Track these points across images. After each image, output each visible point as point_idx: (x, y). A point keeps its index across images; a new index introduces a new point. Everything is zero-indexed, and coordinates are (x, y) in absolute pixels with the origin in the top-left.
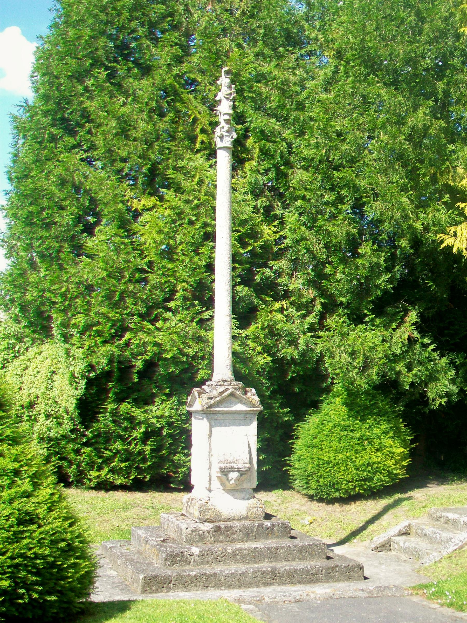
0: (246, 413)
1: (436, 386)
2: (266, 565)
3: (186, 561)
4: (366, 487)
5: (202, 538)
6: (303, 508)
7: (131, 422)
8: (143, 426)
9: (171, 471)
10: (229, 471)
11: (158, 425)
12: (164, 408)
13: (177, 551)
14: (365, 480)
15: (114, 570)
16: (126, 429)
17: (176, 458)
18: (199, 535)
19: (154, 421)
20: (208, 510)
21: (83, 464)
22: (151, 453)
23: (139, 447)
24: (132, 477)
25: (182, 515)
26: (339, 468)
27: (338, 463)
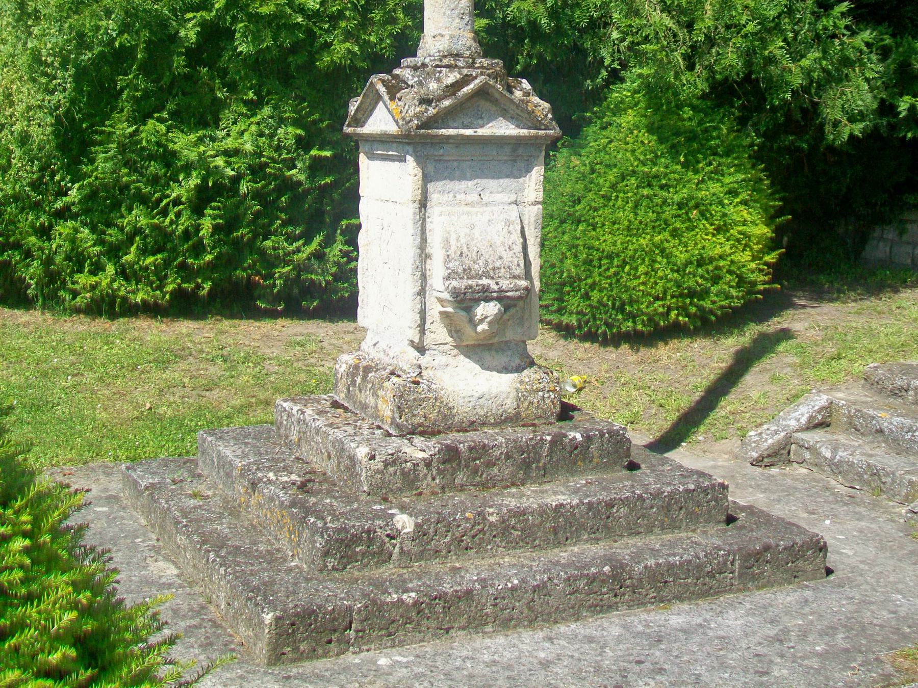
0: (516, 143)
1: (843, 93)
2: (587, 551)
3: (381, 552)
4: (693, 310)
5: (410, 479)
6: (553, 354)
7: (168, 165)
8: (194, 173)
9: (258, 273)
10: (477, 301)
11: (230, 172)
12: (242, 133)
13: (356, 525)
14: (692, 294)
15: (167, 559)
16: (154, 180)
17: (268, 243)
18: (404, 474)
19: (220, 161)
20: (419, 402)
21: (58, 259)
22: (212, 235)
23: (185, 222)
24: (170, 288)
25: (336, 405)
26: (636, 269)
27: (633, 258)
